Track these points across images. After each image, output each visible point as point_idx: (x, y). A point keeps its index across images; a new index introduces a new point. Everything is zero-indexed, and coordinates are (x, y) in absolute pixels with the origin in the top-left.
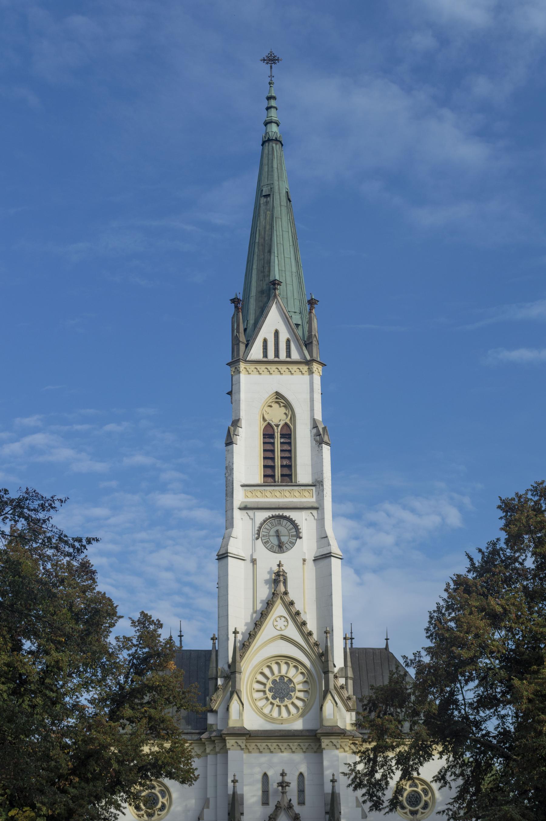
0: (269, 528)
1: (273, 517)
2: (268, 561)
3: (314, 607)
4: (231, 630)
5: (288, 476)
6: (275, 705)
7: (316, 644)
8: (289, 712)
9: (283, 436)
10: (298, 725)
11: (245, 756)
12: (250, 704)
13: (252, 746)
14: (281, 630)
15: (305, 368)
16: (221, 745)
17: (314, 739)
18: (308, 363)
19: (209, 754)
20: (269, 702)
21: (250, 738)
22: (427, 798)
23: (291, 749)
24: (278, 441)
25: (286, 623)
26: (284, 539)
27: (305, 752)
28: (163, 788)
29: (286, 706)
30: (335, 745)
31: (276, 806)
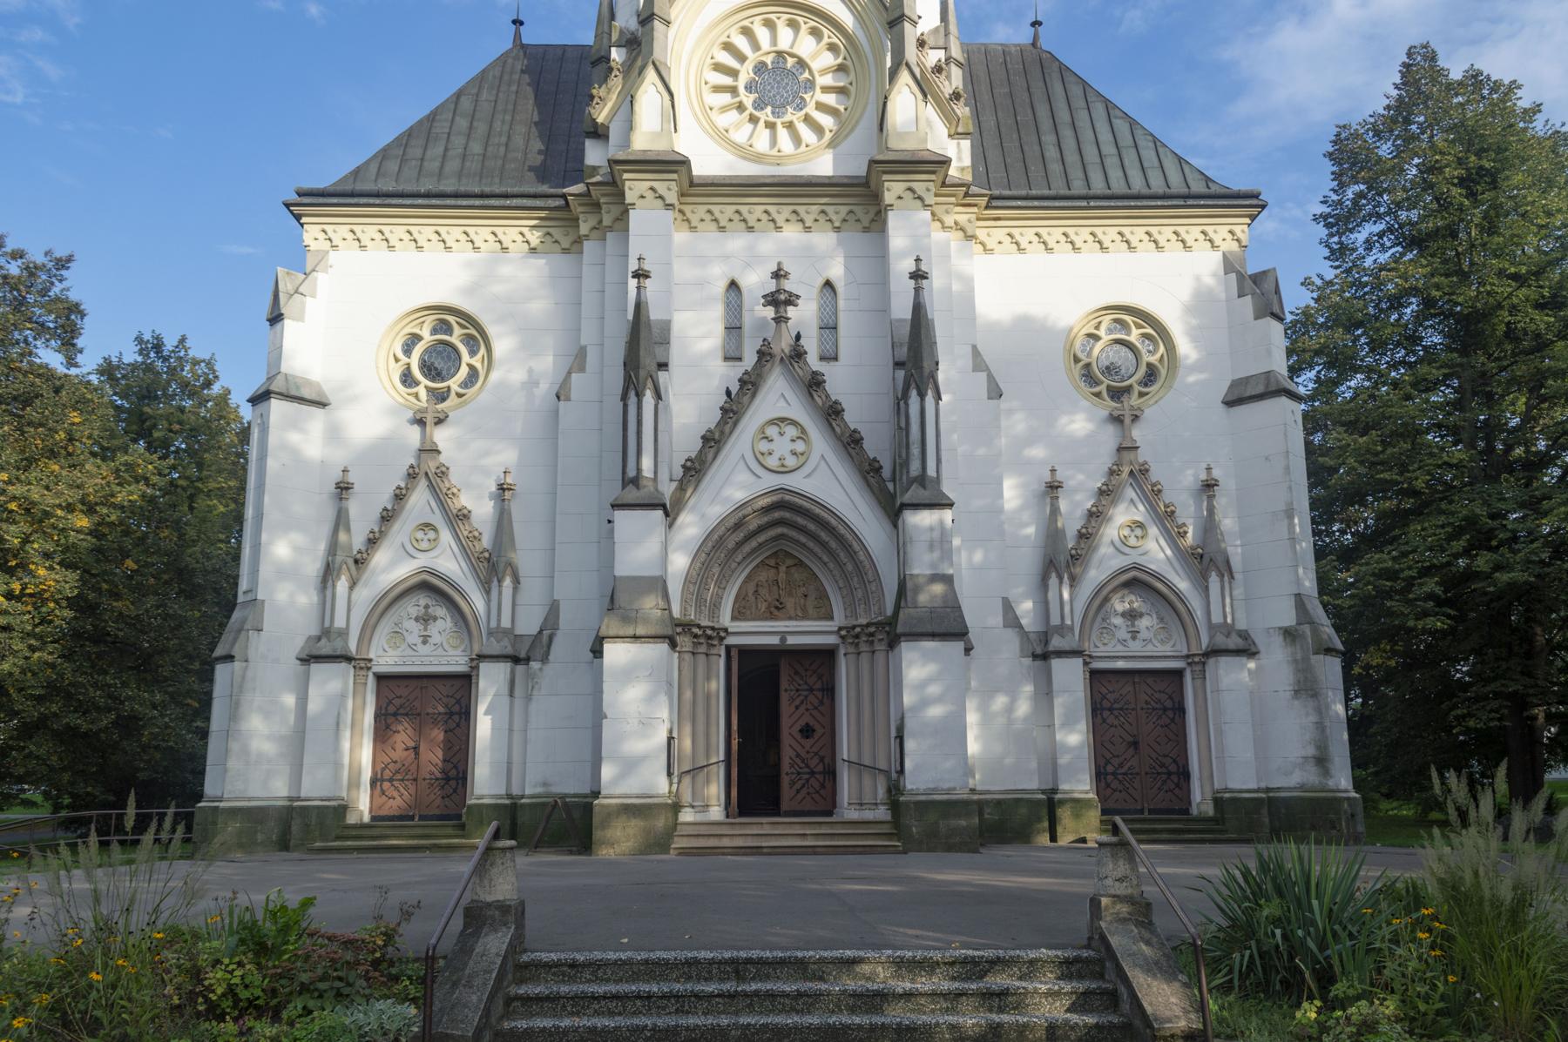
6: (761, 124)
8: (797, 140)
10: (824, 165)
12: (695, 115)
13: (697, 212)
16: (616, 210)
17: (860, 198)
20: (747, 113)
22: (1153, 359)
23: (801, 220)
27: (837, 229)
28: (473, 331)
29: (790, 126)
30: (920, 198)
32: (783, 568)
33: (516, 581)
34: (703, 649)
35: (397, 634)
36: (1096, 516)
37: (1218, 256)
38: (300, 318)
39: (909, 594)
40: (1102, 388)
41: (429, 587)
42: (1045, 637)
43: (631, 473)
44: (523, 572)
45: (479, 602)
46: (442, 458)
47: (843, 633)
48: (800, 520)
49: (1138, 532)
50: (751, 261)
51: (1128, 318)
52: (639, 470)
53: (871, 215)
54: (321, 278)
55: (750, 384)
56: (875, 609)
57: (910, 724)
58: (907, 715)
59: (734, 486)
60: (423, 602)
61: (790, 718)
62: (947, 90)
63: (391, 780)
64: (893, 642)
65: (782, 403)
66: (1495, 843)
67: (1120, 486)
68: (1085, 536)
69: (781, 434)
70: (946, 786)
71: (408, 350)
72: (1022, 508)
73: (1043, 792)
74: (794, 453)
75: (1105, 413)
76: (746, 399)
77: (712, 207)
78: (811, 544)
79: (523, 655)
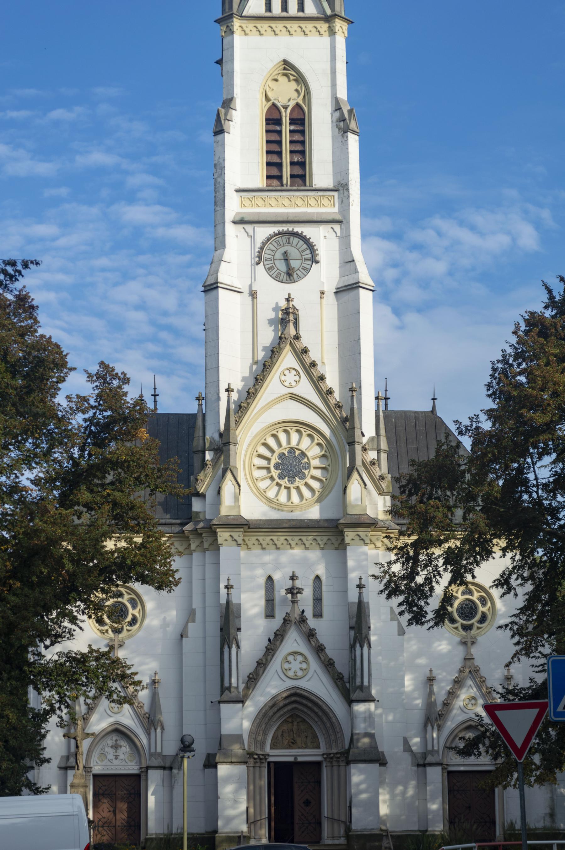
2: (273, 293)
4: (223, 386)
5: (301, 177)
6: (283, 487)
7: (338, 406)
10: (314, 513)
14: (291, 386)
15: (323, 27)
18: (328, 19)
19: (194, 551)
22: (485, 609)
24: (286, 128)
25: (297, 378)
26: (294, 264)
27: (322, 549)
28: (133, 596)
29: (298, 488)
31: (284, 619)
32: (295, 723)
33: (163, 729)
34: (258, 765)
35: (103, 755)
36: (452, 694)
39: (355, 742)
41: (119, 731)
42: (424, 755)
43: (226, 684)
44: (165, 724)
45: (145, 741)
47: (325, 756)
48: (304, 702)
49: (473, 702)
50: (278, 566)
52: (230, 684)
53: (339, 541)
55: (279, 636)
56: (340, 745)
57: (354, 801)
58: (353, 797)
59: (272, 687)
60: (114, 738)
61: (298, 797)
63: (102, 827)
64: (348, 763)
65: (295, 644)
66: (113, 815)
67: (464, 679)
68: (446, 704)
69: (295, 660)
70: (370, 827)
72: (414, 690)
73: (420, 831)
74: (301, 669)
75: (458, 639)
76: (278, 643)
77: (258, 538)
78: (309, 713)
79: (170, 766)
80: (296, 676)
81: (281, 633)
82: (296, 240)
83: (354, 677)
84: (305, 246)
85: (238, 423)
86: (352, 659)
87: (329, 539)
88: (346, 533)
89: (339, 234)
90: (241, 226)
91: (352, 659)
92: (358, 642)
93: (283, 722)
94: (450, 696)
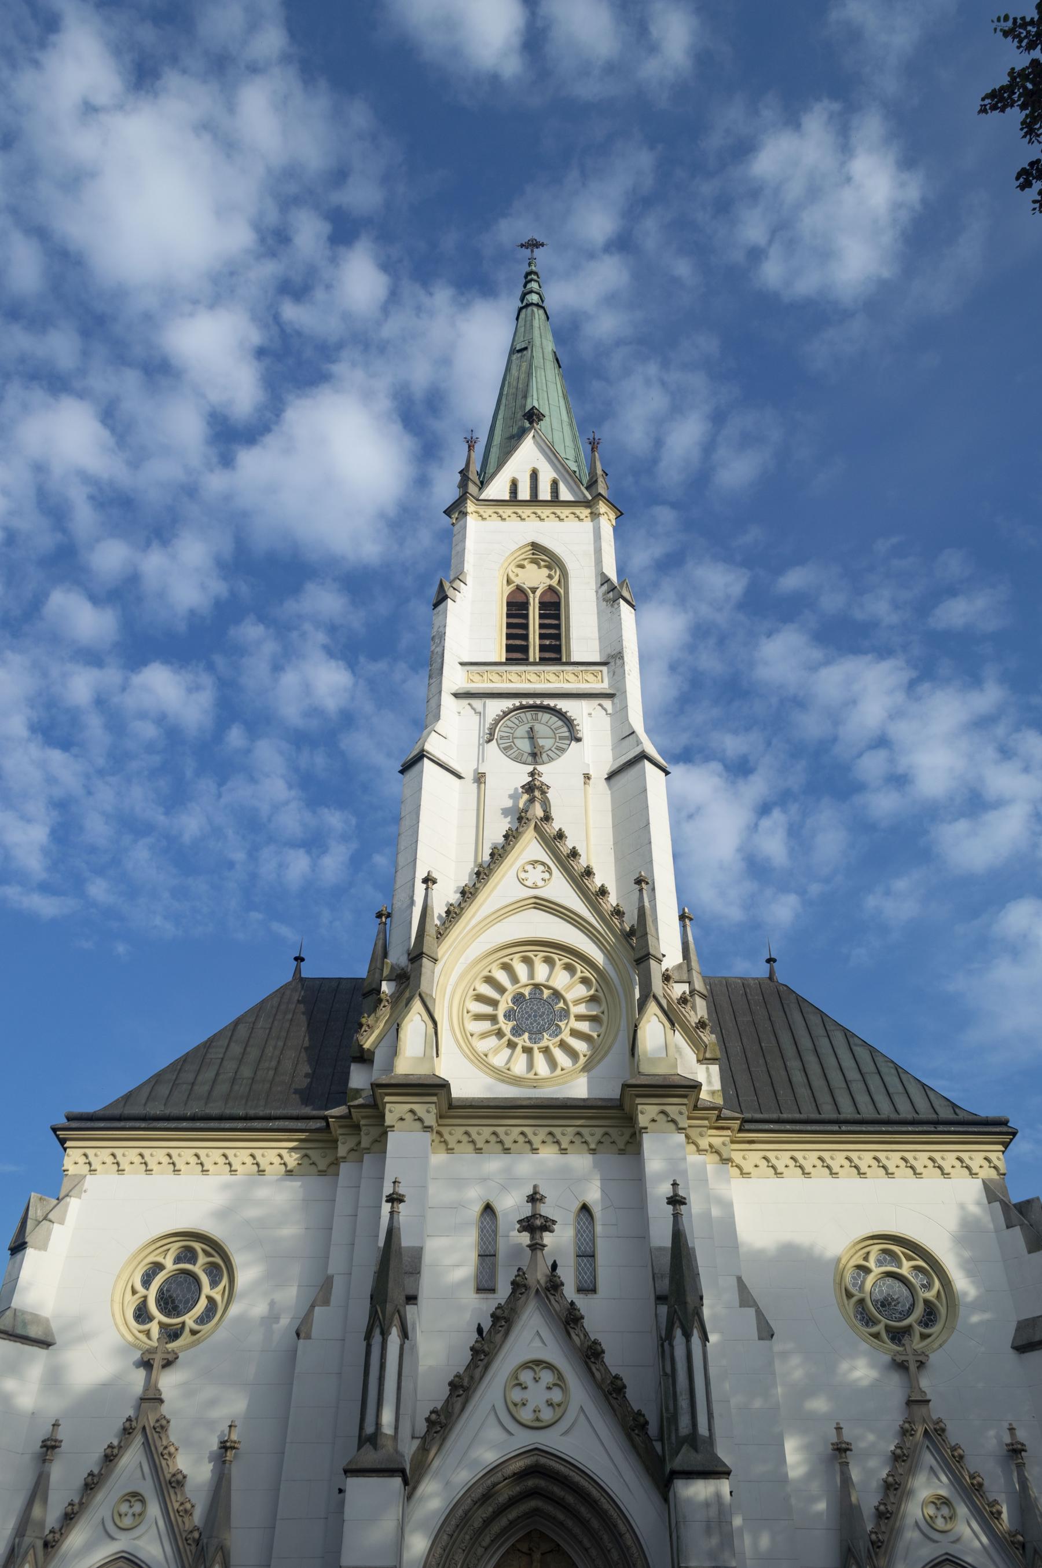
0: (513, 725)
1: (522, 707)
3: (608, 821)
4: (421, 874)
5: (554, 651)
6: (519, 1049)
7: (618, 912)
8: (553, 1063)
9: (543, 605)
10: (579, 1088)
11: (438, 1159)
12: (457, 1041)
13: (455, 1134)
14: (536, 887)
15: (584, 512)
17: (614, 1120)
18: (587, 504)
19: (344, 1159)
20: (505, 1039)
21: (453, 1112)
22: (930, 1295)
25: (546, 876)
26: (545, 743)
27: (593, 1151)
28: (218, 1260)
29: (546, 1051)
31: (513, 1283)
32: (537, 1556)
36: (894, 1488)
37: (977, 1185)
38: (44, 1247)
40: (880, 1328)
43: (369, 1429)
46: (165, 1409)
49: (945, 1511)
50: (509, 1182)
51: (896, 1249)
52: (378, 1425)
53: (626, 1137)
54: (74, 1205)
55: (503, 1320)
59: (484, 1446)
62: (694, 1019)
65: (537, 1343)
68: (886, 1515)
69: (536, 1380)
71: (146, 1282)
72: (809, 1476)
74: (550, 1404)
75: (887, 1358)
80: (538, 1420)
81: (505, 1315)
82: (546, 717)
83: (674, 1418)
84: (560, 723)
85: (440, 935)
86: (666, 1374)
87: (606, 1134)
88: (640, 1107)
89: (610, 711)
90: (464, 702)
91: (666, 1374)
92: (677, 1324)
93: (507, 1552)
94: (891, 1493)
